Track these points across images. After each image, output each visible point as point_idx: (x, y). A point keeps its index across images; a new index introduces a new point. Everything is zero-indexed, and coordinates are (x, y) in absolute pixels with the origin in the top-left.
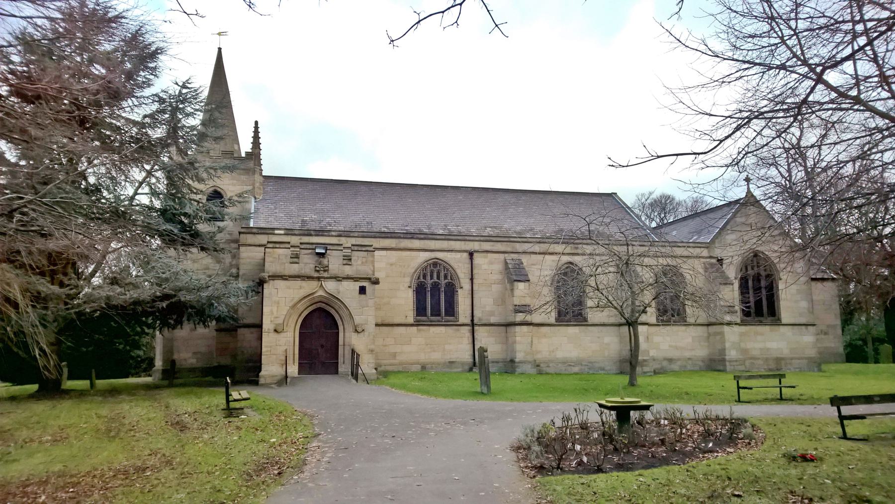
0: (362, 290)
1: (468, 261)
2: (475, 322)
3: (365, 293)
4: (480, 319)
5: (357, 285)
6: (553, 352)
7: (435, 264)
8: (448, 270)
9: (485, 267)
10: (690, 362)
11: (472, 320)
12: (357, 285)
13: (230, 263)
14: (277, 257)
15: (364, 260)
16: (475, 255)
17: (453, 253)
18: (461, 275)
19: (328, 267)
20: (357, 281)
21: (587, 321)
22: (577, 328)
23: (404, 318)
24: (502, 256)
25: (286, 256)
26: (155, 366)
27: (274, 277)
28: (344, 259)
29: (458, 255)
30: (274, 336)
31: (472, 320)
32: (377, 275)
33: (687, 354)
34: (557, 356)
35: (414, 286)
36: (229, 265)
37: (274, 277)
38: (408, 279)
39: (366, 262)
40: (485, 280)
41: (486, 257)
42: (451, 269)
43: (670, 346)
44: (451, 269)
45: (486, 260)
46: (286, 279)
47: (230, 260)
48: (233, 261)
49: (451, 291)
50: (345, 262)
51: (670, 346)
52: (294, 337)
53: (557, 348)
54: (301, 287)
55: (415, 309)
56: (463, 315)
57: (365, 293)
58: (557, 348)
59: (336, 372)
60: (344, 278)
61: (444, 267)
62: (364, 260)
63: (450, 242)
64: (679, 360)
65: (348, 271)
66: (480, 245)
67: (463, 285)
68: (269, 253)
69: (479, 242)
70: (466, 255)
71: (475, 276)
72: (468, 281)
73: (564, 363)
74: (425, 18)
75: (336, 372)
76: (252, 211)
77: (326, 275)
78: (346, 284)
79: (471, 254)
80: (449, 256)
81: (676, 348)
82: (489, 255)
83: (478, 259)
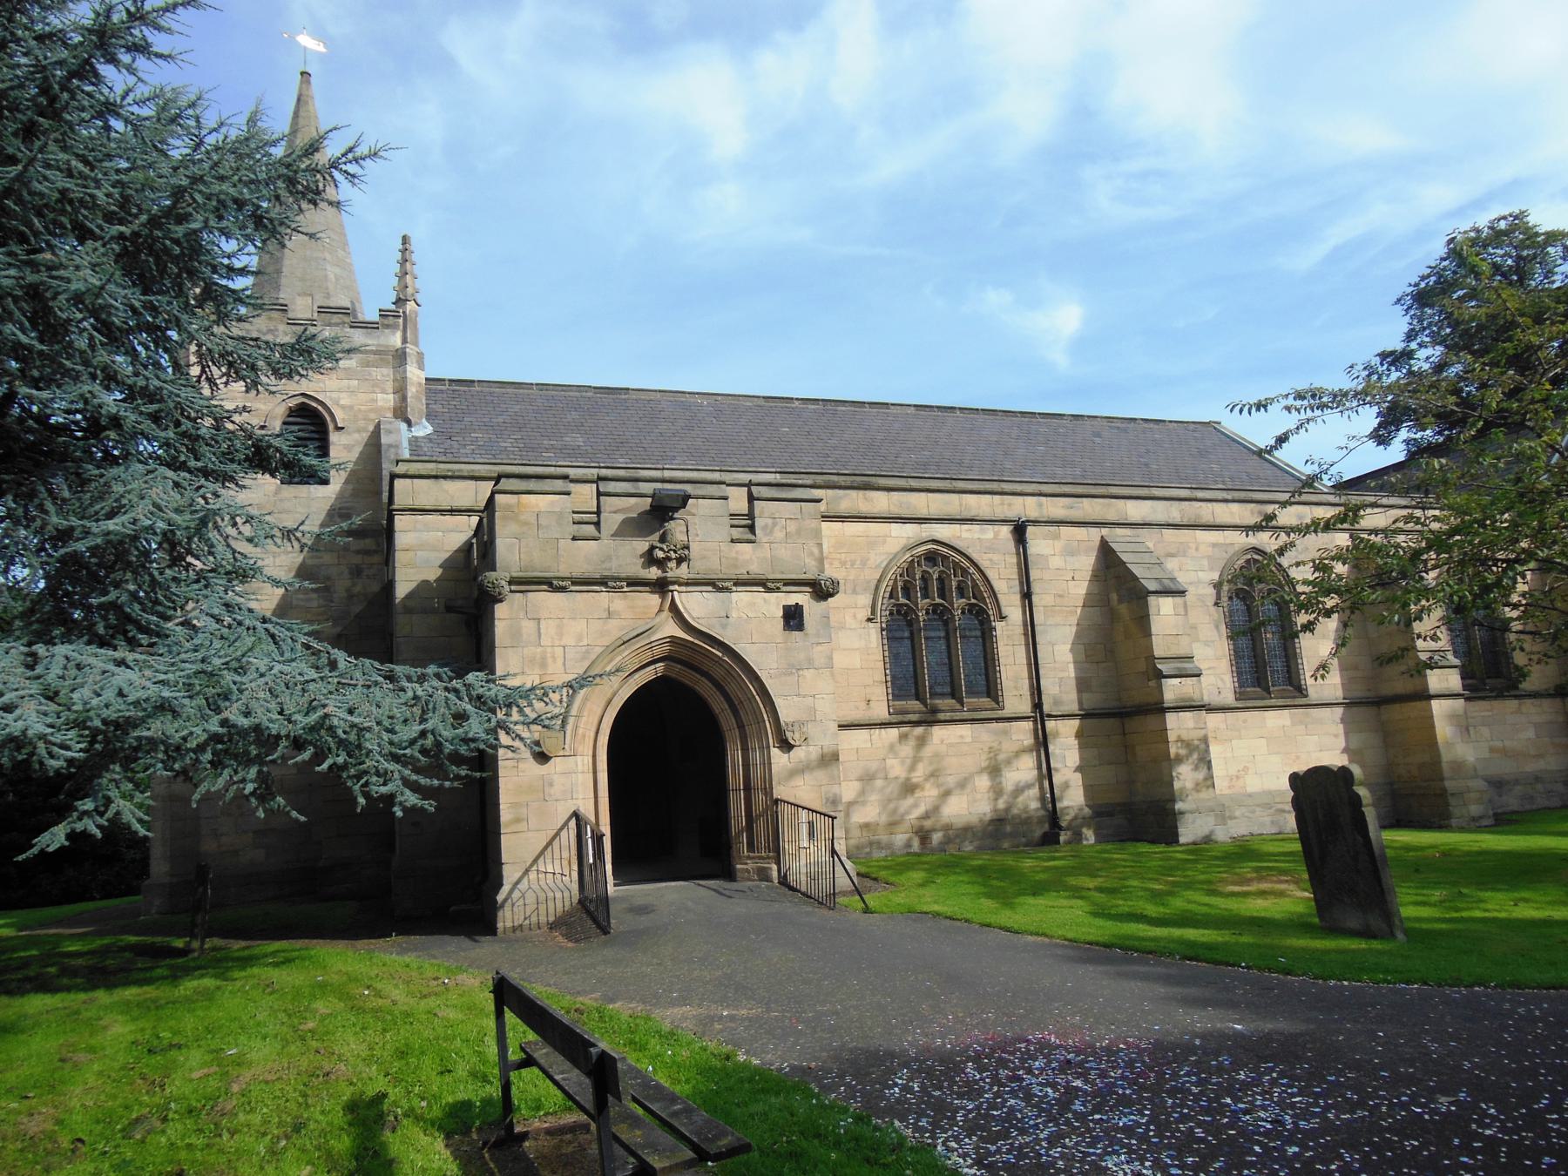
0: (793, 618)
1: (1011, 545)
2: (1046, 708)
3: (800, 627)
4: (1057, 702)
5: (774, 604)
6: (1238, 777)
7: (931, 557)
8: (965, 572)
9: (1056, 562)
10: (1539, 787)
11: (1038, 705)
12: (774, 604)
13: (348, 590)
14: (533, 520)
15: (792, 527)
16: (1030, 530)
17: (976, 527)
18: (1000, 586)
19: (687, 548)
20: (777, 590)
21: (1306, 696)
22: (1286, 712)
23: (863, 705)
24: (1095, 534)
25: (560, 515)
26: (148, 876)
27: (525, 583)
28: (732, 526)
29: (989, 532)
30: (531, 767)
31: (1038, 705)
32: (831, 571)
33: (1531, 767)
34: (1249, 790)
35: (883, 615)
36: (345, 595)
37: (525, 583)
38: (865, 600)
39: (799, 532)
40: (1060, 596)
41: (1057, 537)
42: (972, 570)
43: (1492, 750)
44: (972, 570)
45: (1059, 545)
46: (562, 589)
47: (348, 583)
48: (354, 585)
49: (982, 619)
50: (736, 533)
51: (1492, 750)
52: (595, 772)
53: (1246, 769)
54: (610, 615)
55: (889, 678)
56: (1016, 697)
57: (800, 627)
58: (1246, 769)
59: (729, 874)
60: (739, 583)
61: (956, 564)
62: (792, 527)
63: (964, 496)
64: (1517, 782)
65: (750, 559)
66: (1040, 505)
67: (1005, 611)
68: (508, 507)
69: (1035, 499)
70: (1005, 531)
71: (1036, 588)
72: (1016, 599)
73: (1267, 806)
74: (452, 511)
75: (729, 874)
76: (406, 455)
77: (683, 572)
78: (742, 599)
79: (1019, 531)
80: (965, 535)
81: (1504, 753)
82: (1064, 530)
83: (1037, 541)
